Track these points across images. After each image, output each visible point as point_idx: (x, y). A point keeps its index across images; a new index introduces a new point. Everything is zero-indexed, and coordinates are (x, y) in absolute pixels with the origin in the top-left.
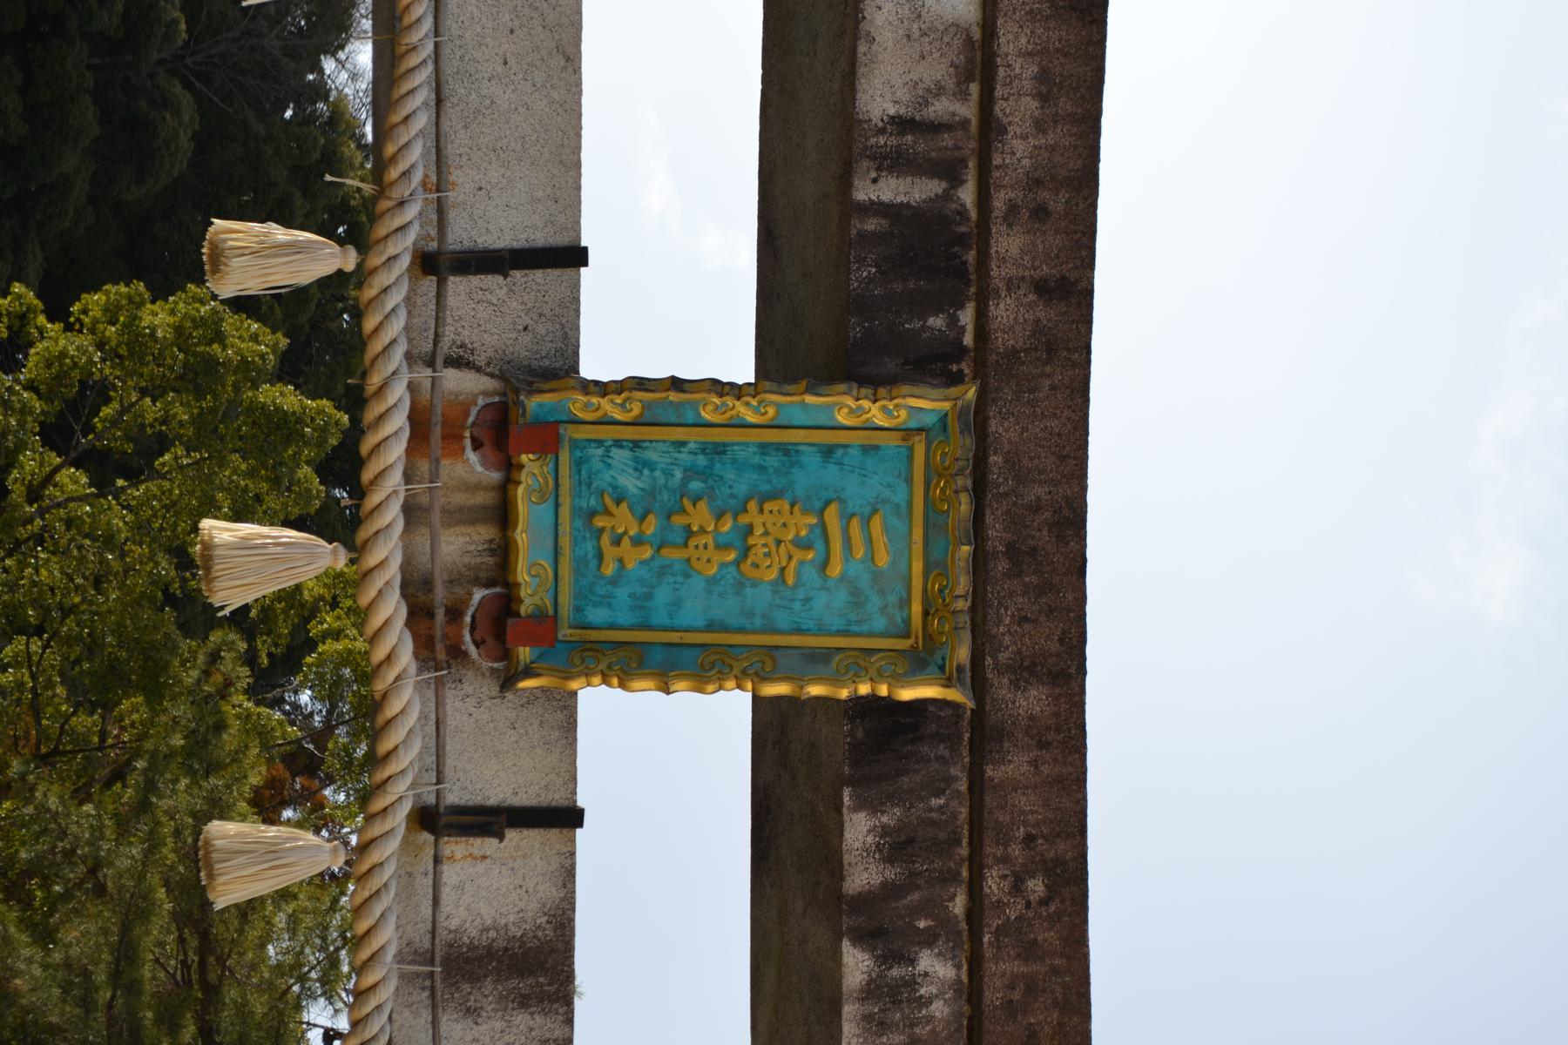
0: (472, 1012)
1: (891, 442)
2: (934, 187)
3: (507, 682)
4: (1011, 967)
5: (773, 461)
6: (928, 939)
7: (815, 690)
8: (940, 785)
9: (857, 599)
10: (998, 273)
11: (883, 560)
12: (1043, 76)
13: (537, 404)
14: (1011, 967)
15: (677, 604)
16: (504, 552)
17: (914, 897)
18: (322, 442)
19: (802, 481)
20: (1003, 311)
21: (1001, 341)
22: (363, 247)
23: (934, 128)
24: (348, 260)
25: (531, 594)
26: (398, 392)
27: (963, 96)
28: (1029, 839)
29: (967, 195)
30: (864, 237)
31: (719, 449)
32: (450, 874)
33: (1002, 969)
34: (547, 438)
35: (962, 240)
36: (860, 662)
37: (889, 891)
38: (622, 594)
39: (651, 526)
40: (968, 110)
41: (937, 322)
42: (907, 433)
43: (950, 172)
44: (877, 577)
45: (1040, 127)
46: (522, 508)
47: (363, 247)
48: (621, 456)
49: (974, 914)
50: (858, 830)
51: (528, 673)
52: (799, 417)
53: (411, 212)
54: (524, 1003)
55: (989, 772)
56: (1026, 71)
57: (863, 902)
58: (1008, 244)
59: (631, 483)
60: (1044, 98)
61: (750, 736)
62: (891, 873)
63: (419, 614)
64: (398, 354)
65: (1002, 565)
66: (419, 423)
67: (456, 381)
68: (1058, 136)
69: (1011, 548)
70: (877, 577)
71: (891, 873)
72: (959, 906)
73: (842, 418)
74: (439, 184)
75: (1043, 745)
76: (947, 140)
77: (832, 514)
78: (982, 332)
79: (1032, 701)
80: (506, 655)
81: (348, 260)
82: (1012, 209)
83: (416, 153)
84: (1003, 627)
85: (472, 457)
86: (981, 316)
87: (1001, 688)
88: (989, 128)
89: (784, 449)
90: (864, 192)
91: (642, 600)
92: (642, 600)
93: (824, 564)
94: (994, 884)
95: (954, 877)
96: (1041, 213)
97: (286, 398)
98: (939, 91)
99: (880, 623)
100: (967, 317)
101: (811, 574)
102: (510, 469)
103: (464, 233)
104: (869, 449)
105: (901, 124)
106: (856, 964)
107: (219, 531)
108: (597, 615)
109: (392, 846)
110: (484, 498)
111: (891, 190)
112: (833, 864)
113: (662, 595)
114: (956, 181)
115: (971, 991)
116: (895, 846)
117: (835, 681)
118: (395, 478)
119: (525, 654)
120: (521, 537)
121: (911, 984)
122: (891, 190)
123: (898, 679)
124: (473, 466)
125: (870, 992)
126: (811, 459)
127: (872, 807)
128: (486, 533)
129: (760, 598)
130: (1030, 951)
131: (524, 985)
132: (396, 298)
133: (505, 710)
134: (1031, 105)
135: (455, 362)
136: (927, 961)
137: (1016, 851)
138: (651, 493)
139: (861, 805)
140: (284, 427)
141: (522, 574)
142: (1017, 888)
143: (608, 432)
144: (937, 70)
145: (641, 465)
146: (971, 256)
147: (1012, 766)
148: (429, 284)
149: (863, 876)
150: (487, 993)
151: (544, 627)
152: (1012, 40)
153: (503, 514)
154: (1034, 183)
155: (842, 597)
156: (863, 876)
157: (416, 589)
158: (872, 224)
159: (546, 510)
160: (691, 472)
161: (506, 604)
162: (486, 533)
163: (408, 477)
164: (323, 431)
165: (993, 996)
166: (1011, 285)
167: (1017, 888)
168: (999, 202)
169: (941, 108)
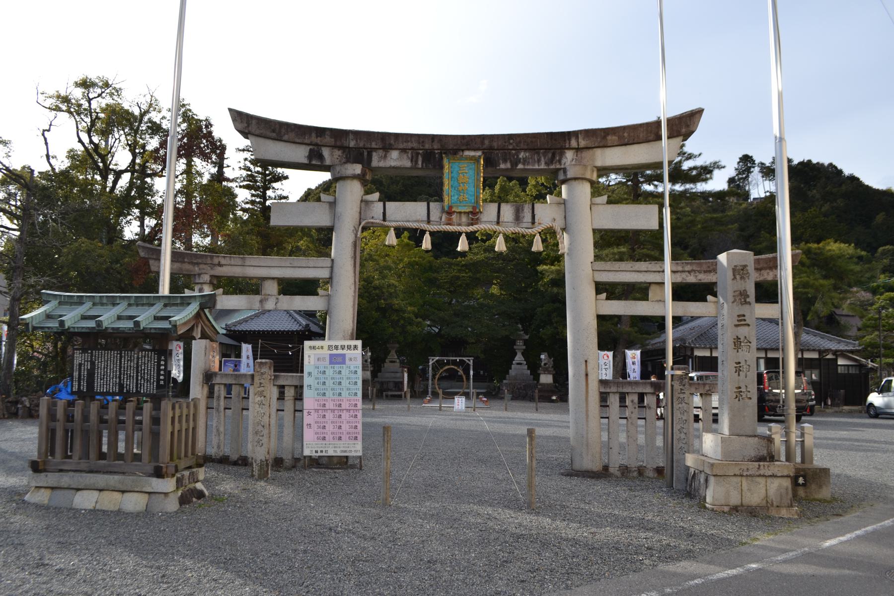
0: (524, 217)
1: (450, 164)
2: (420, 157)
3: (481, 212)
4: (522, 145)
5: (453, 179)
6: (518, 156)
7: (482, 175)
8: (497, 154)
9: (470, 169)
10: (431, 148)
11: (466, 165)
12: (405, 142)
13: (446, 209)
14: (522, 145)
15: (472, 191)
16: (465, 213)
17: (512, 158)
18: (505, 181)
19: (456, 176)
20: (435, 147)
21: (439, 147)
22: (426, 231)
23: (412, 157)
24: (428, 233)
25: (471, 210)
26: (443, 227)
27: (408, 152)
28: (505, 142)
29: (421, 152)
30: (426, 166)
31: (452, 186)
32: (505, 220)
33: (522, 146)
34: (450, 207)
35: (427, 152)
36: (478, 168)
37: (511, 162)
38: (470, 198)
39: (462, 194)
40: (410, 152)
41: (437, 156)
42: (449, 163)
43: (418, 154)
44: (468, 166)
45: (412, 142)
46: (459, 211)
47: (426, 231)
48: (453, 198)
49: (515, 150)
50: (502, 166)
51: (480, 210)
52: (447, 177)
53: (422, 225)
54: (523, 210)
55: (496, 148)
56: (405, 144)
57: (512, 165)
58: (427, 146)
59: (456, 197)
60: (408, 142)
61: (537, 132)
62: (508, 161)
63: (472, 224)
64: (439, 227)
65: (469, 147)
66: (447, 224)
67: (443, 219)
68: (413, 139)
69: (467, 145)
70: (468, 166)
71: (508, 161)
72: (514, 152)
73: (447, 171)
74: (418, 221)
75: (493, 140)
76: (414, 155)
77: (460, 172)
78: (438, 149)
79: (487, 142)
80: (478, 213)
81: (428, 233)
82: (422, 146)
83: (415, 224)
84: (477, 146)
85: (453, 216)
86: (436, 150)
87: (485, 146)
88: (412, 149)
89: (452, 178)
90: (420, 166)
91: (471, 195)
92: (471, 195)
93: (466, 173)
94: (511, 147)
95: (510, 152)
96: (423, 142)
97: (497, 187)
98: (408, 156)
99: (474, 166)
100: (436, 151)
101: (468, 175)
102: (454, 212)
103: (425, 218)
104: (451, 167)
105: (412, 161)
106: (520, 166)
107: (459, 249)
108: (473, 201)
109: (500, 228)
110: (458, 215)
111: (420, 163)
112: (507, 170)
113: (470, 193)
114: (419, 153)
115: (525, 150)
116: (505, 161)
117: (481, 172)
118: (454, 227)
119: (477, 210)
120: (463, 211)
121: (524, 158)
122: (420, 163)
123: (480, 164)
124: (454, 216)
125: (524, 164)
126: (453, 174)
127: (500, 164)
128: (462, 215)
129: (470, 181)
130: (520, 142)
131: (521, 210)
132: (432, 227)
133: (485, 213)
134: (409, 143)
135: (441, 220)
136: (521, 156)
137: (506, 144)
138: (457, 194)
139: (499, 166)
140: (503, 188)
141: (467, 211)
142: (511, 144)
143: (450, 200)
144: (405, 156)
145: (454, 196)
146: (429, 151)
147: (495, 145)
148: (431, 222)
149: (508, 165)
150: (521, 215)
151: (474, 208)
152: (401, 146)
153: (460, 213)
154: (419, 143)
155: (470, 171)
156: (508, 165)
157: (469, 225)
158: (424, 165)
159: (460, 207)
160: (455, 189)
161: (471, 212)
162: (462, 215)
163: (454, 225)
164: (504, 181)
165: (526, 147)
166: (432, 146)
167: (511, 144)
168: (421, 148)
169: (410, 155)
